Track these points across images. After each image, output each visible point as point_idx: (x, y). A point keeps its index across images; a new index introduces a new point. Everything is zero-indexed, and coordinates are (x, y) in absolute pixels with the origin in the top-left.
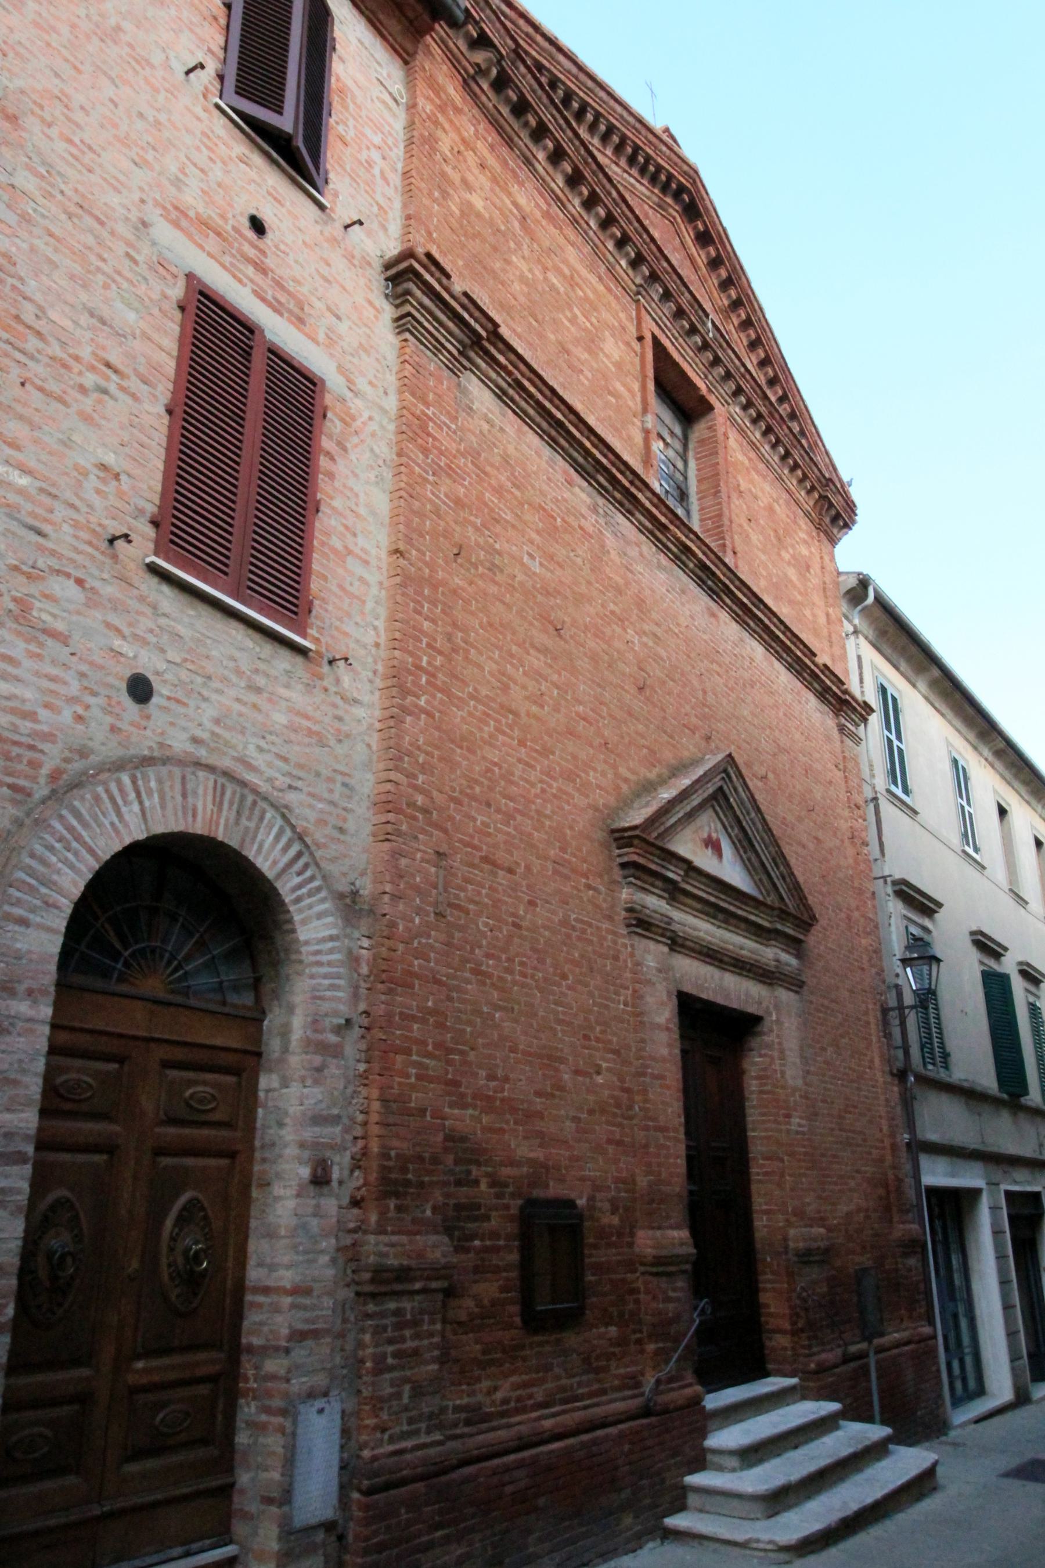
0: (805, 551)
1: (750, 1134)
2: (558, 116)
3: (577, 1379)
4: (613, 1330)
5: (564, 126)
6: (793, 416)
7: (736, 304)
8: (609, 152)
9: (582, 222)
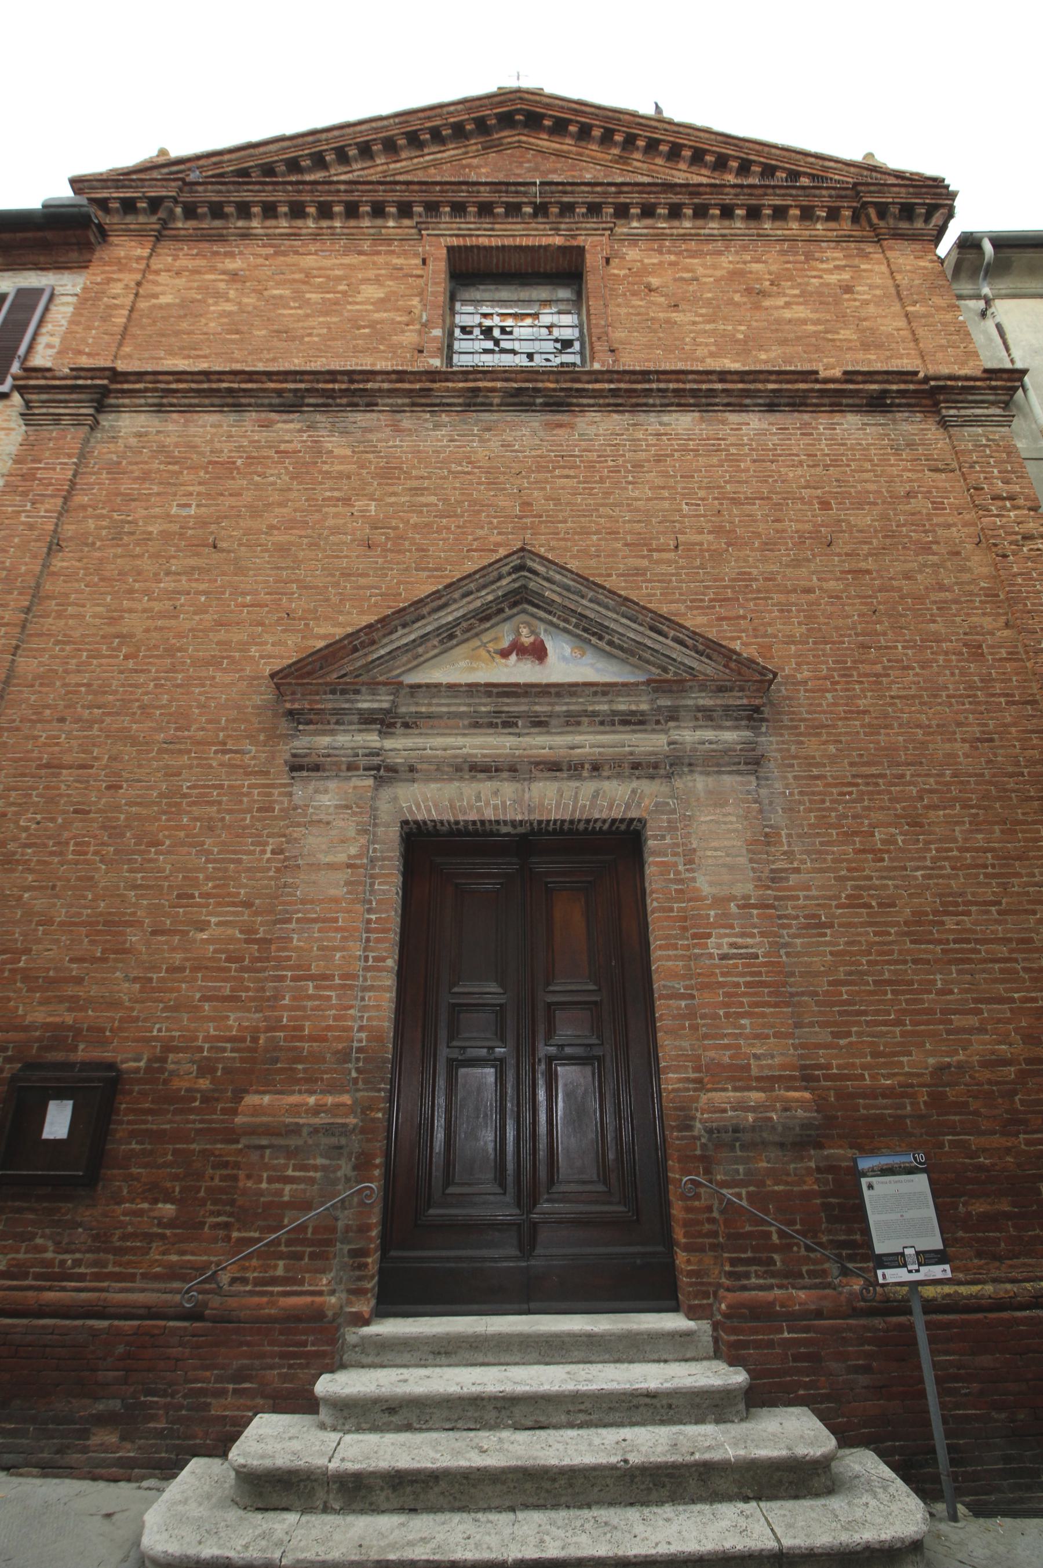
2: (250, 187)
3: (78, 1256)
6: (769, 171)
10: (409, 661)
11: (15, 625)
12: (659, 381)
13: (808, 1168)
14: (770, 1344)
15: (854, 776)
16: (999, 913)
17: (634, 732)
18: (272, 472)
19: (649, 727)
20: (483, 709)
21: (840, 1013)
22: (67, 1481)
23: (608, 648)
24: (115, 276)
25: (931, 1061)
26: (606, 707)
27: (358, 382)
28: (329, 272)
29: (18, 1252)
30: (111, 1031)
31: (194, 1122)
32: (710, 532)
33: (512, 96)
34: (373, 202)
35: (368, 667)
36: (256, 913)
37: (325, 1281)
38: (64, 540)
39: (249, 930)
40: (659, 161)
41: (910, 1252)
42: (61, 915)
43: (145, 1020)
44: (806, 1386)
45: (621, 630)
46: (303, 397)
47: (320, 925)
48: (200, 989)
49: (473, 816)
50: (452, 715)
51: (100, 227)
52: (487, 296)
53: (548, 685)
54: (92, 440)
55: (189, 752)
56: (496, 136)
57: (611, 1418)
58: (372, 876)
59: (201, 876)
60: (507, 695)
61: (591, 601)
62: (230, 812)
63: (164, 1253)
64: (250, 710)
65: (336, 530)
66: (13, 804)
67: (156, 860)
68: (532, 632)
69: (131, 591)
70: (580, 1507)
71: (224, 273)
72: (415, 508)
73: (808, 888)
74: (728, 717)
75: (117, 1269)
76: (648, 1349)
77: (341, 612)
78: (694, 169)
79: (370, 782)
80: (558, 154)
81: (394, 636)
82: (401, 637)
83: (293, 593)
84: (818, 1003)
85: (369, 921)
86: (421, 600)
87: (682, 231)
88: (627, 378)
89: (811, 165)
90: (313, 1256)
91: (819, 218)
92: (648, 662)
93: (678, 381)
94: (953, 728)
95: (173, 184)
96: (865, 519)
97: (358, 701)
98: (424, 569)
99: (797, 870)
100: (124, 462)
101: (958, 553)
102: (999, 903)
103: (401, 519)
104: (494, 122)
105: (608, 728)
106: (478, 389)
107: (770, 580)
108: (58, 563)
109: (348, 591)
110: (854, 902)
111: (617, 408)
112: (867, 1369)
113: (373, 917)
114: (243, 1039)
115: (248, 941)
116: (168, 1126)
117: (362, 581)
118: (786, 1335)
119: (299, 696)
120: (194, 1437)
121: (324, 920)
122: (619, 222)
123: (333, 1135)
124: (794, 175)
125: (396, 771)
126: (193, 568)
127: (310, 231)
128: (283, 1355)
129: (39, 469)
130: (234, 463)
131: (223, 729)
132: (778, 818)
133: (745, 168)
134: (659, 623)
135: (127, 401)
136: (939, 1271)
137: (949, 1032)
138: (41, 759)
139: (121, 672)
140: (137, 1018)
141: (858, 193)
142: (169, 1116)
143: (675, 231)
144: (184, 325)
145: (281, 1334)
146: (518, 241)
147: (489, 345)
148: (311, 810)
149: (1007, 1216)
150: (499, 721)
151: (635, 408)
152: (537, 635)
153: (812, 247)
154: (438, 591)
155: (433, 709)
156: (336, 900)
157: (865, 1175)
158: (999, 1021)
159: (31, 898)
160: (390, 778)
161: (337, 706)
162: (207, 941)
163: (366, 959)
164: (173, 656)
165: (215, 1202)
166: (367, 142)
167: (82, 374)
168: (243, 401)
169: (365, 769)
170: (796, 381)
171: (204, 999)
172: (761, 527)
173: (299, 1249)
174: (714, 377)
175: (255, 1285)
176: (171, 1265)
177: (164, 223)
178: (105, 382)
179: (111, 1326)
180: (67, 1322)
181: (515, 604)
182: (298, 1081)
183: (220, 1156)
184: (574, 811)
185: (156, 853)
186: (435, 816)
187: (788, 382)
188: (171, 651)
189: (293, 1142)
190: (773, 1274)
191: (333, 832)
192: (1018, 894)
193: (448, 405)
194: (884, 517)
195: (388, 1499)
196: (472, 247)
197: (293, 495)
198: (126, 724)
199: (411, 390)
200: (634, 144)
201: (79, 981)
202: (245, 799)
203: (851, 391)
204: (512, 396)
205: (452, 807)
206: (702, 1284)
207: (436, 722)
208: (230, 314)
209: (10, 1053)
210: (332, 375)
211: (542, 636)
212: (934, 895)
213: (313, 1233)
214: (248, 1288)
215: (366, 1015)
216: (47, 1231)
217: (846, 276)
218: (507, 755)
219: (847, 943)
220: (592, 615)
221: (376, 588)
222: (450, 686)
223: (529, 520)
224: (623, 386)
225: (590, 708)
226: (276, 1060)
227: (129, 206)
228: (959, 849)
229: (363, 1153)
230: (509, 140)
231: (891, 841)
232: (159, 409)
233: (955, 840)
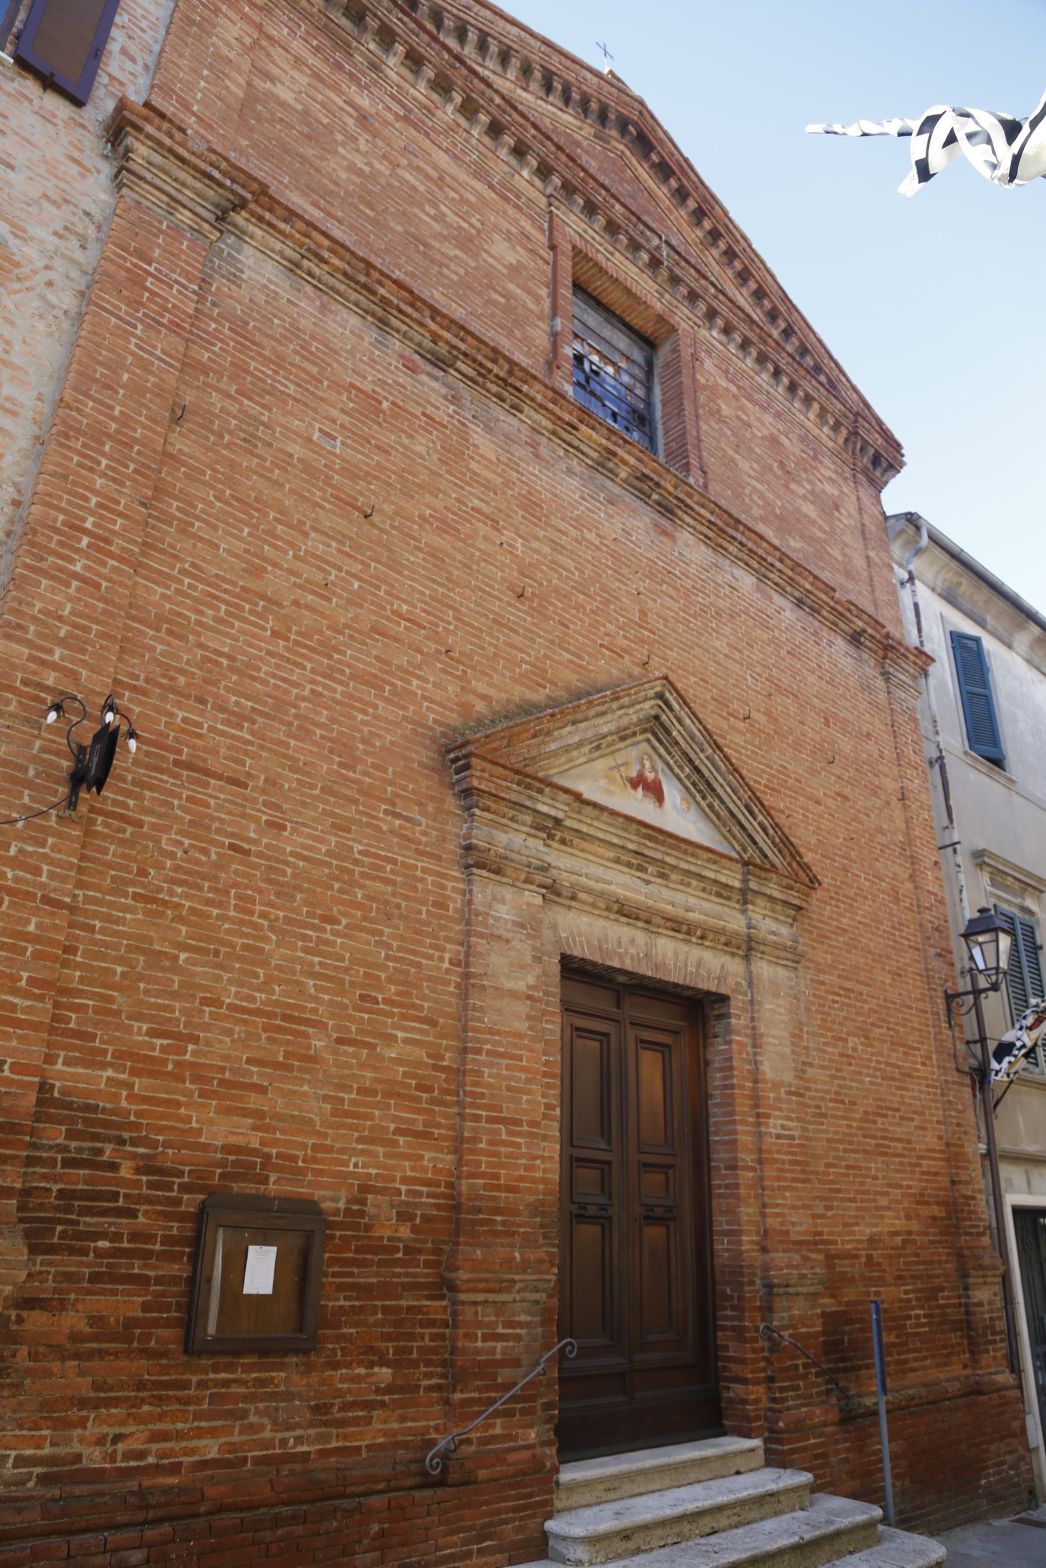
0: (830, 489)
3: (298, 1432)
4: (385, 1373)
5: (417, 29)
6: (804, 351)
7: (714, 235)
12: (743, 534)
15: (841, 988)
23: (707, 810)
29: (231, 1434)
31: (399, 1275)
32: (764, 714)
36: (441, 1036)
48: (395, 1119)
61: (707, 758)
62: (407, 898)
63: (385, 1422)
75: (341, 1444)
79: (539, 900)
106: (615, 454)
114: (437, 1184)
115: (436, 1068)
116: (374, 1280)
130: (380, 403)
131: (391, 783)
152: (656, 772)
156: (520, 1036)
162: (399, 1061)
171: (398, 1131)
178: (249, 196)
191: (513, 954)
193: (583, 453)
201: (262, 1090)
205: (601, 948)
209: (186, 1179)
211: (661, 776)
216: (261, 1406)
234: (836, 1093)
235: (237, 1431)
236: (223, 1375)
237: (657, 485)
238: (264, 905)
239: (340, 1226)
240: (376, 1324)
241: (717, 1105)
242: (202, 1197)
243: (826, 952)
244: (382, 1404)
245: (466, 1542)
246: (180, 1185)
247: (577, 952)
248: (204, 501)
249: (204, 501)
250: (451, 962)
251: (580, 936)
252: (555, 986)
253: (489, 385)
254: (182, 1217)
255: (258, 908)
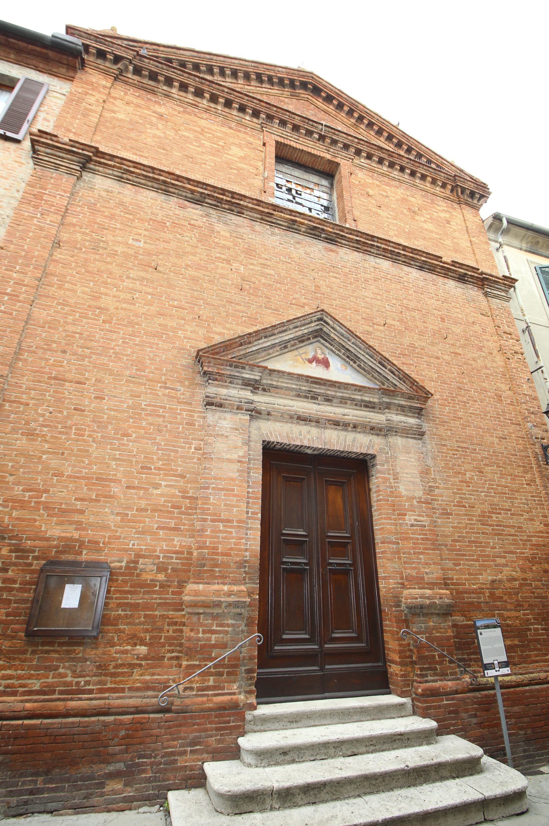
1: (375, 528)
2: (175, 71)
3: (88, 679)
4: (143, 650)
5: (181, 73)
6: (419, 156)
7: (361, 119)
8: (241, 81)
9: (212, 109)
10: (265, 356)
11: (33, 287)
12: (378, 242)
13: (449, 625)
14: (439, 707)
15: (458, 447)
16: (511, 514)
17: (369, 411)
18: (187, 234)
19: (376, 411)
20: (304, 388)
21: (456, 555)
22: (92, 815)
23: (358, 368)
24: (90, 92)
25: (490, 578)
26: (359, 397)
27: (236, 199)
28: (214, 133)
29: (48, 678)
30: (103, 543)
31: (156, 599)
32: (398, 321)
33: (309, 75)
34: (240, 103)
35: (245, 355)
36: (188, 482)
37: (235, 687)
38: (62, 242)
39: (184, 491)
40: (372, 133)
41: (496, 662)
42: (68, 471)
43: (125, 538)
44: (453, 725)
45: (366, 360)
46: (205, 198)
47: (225, 492)
48: (157, 522)
49: (298, 443)
50: (288, 389)
51: (83, 59)
52: (288, 171)
53: (335, 382)
54: (77, 186)
55: (145, 384)
56: (297, 91)
57: (384, 747)
58: (248, 468)
59: (155, 457)
60: (316, 383)
61: (353, 343)
62: (171, 423)
64: (179, 366)
65: (223, 276)
66: (33, 399)
67: (128, 445)
68: (323, 353)
69: (106, 283)
70: (388, 791)
71: (155, 112)
72: (263, 274)
73: (442, 496)
74: (411, 411)
75: (113, 686)
76: (386, 712)
77: (227, 322)
78: (386, 142)
79: (248, 417)
80: (326, 112)
81: (260, 342)
82: (264, 342)
83: (201, 306)
84: (448, 550)
85: (248, 492)
86: (275, 326)
87: (382, 171)
88: (365, 236)
89: (437, 160)
90: (229, 674)
91: (438, 185)
92: (376, 378)
93: (386, 245)
94: (492, 431)
95: (131, 52)
96: (457, 330)
97: (243, 373)
98: (269, 308)
99: (438, 487)
100: (99, 205)
101: (492, 354)
102: (511, 510)
103: (256, 278)
104: (298, 84)
105: (358, 408)
106: (296, 221)
107: (423, 349)
108: (57, 255)
109: (231, 311)
110: (460, 505)
111: (357, 250)
112: (475, 716)
113: (250, 490)
114: (182, 553)
115: (183, 497)
116: (141, 601)
117: (238, 307)
118: (445, 702)
119: (212, 364)
120: (169, 780)
121: (227, 490)
122: (357, 157)
123: (238, 607)
124: (429, 161)
125: (260, 414)
126: (143, 278)
127: (204, 106)
128: (217, 729)
129: (45, 194)
130: (165, 223)
131: (164, 375)
132: (430, 462)
133: (409, 150)
134: (384, 361)
135: (101, 169)
136: (506, 671)
137: (496, 565)
138: (51, 373)
139: (102, 330)
140: (120, 537)
141: (455, 179)
142: (141, 595)
143: (379, 170)
144: (133, 135)
145: (216, 717)
146: (309, 150)
147: (291, 198)
148: (217, 428)
149: (517, 646)
150: (310, 395)
151: (365, 252)
152: (325, 354)
153: (434, 197)
154: (283, 323)
155: (279, 384)
156: (233, 479)
157: (479, 629)
158: (512, 561)
159: (48, 459)
160: (257, 417)
161: (232, 373)
162: (162, 495)
163: (247, 512)
164: (133, 327)
165: (170, 645)
166: (236, 70)
167: (77, 145)
168: (171, 190)
169: (246, 410)
170: (433, 259)
171: (159, 528)
172: (418, 324)
173: (221, 670)
174: (401, 248)
175: (198, 691)
176: (146, 682)
177: (121, 72)
178: (91, 154)
179: (115, 720)
180: (86, 719)
181: (316, 337)
182: (216, 577)
183: (172, 618)
184: (345, 446)
185: (127, 441)
186: (280, 440)
187: (430, 259)
188: (131, 324)
189: (216, 611)
190: (436, 675)
191: (230, 442)
192: (517, 507)
193: (279, 225)
194: (465, 331)
195: (302, 799)
196: (287, 145)
197: (199, 251)
198: (105, 362)
199: (263, 212)
200: (362, 121)
201: (82, 512)
202: (179, 417)
203: (453, 270)
204: (311, 229)
205: (288, 437)
206: (407, 680)
207: (279, 391)
208: (159, 137)
209: (36, 554)
210: (223, 191)
211: (327, 356)
212: (488, 504)
213: (228, 661)
214: (194, 693)
215: (249, 543)
216: (67, 664)
217: (447, 216)
218: (314, 414)
219: (458, 523)
220: (353, 351)
221: (245, 312)
222: (289, 374)
223: (319, 295)
224: (362, 239)
225: (353, 397)
226: (204, 565)
227: (101, 54)
228: (497, 485)
229: (250, 617)
230: (303, 96)
231: (472, 478)
232: (120, 179)
233: (495, 481)
234: (457, 502)
235: (51, 676)
236: (46, 648)
237: (323, 230)
238: (90, 431)
239: (122, 574)
240: (140, 623)
241: (376, 510)
242: (44, 562)
243: (447, 430)
244: (140, 666)
245: (182, 745)
246: (33, 557)
247: (272, 439)
248: (71, 275)
249: (71, 275)
250: (195, 449)
251: (275, 431)
252: (259, 456)
253: (224, 206)
254: (32, 572)
255: (87, 433)
